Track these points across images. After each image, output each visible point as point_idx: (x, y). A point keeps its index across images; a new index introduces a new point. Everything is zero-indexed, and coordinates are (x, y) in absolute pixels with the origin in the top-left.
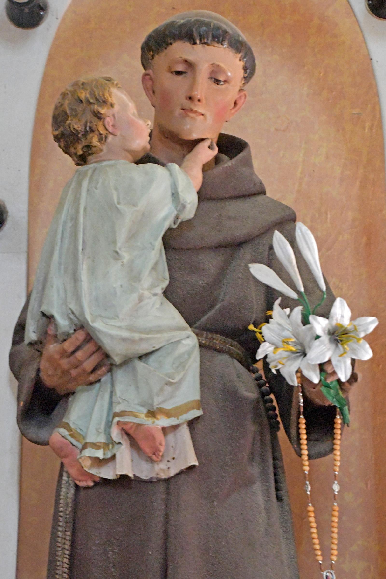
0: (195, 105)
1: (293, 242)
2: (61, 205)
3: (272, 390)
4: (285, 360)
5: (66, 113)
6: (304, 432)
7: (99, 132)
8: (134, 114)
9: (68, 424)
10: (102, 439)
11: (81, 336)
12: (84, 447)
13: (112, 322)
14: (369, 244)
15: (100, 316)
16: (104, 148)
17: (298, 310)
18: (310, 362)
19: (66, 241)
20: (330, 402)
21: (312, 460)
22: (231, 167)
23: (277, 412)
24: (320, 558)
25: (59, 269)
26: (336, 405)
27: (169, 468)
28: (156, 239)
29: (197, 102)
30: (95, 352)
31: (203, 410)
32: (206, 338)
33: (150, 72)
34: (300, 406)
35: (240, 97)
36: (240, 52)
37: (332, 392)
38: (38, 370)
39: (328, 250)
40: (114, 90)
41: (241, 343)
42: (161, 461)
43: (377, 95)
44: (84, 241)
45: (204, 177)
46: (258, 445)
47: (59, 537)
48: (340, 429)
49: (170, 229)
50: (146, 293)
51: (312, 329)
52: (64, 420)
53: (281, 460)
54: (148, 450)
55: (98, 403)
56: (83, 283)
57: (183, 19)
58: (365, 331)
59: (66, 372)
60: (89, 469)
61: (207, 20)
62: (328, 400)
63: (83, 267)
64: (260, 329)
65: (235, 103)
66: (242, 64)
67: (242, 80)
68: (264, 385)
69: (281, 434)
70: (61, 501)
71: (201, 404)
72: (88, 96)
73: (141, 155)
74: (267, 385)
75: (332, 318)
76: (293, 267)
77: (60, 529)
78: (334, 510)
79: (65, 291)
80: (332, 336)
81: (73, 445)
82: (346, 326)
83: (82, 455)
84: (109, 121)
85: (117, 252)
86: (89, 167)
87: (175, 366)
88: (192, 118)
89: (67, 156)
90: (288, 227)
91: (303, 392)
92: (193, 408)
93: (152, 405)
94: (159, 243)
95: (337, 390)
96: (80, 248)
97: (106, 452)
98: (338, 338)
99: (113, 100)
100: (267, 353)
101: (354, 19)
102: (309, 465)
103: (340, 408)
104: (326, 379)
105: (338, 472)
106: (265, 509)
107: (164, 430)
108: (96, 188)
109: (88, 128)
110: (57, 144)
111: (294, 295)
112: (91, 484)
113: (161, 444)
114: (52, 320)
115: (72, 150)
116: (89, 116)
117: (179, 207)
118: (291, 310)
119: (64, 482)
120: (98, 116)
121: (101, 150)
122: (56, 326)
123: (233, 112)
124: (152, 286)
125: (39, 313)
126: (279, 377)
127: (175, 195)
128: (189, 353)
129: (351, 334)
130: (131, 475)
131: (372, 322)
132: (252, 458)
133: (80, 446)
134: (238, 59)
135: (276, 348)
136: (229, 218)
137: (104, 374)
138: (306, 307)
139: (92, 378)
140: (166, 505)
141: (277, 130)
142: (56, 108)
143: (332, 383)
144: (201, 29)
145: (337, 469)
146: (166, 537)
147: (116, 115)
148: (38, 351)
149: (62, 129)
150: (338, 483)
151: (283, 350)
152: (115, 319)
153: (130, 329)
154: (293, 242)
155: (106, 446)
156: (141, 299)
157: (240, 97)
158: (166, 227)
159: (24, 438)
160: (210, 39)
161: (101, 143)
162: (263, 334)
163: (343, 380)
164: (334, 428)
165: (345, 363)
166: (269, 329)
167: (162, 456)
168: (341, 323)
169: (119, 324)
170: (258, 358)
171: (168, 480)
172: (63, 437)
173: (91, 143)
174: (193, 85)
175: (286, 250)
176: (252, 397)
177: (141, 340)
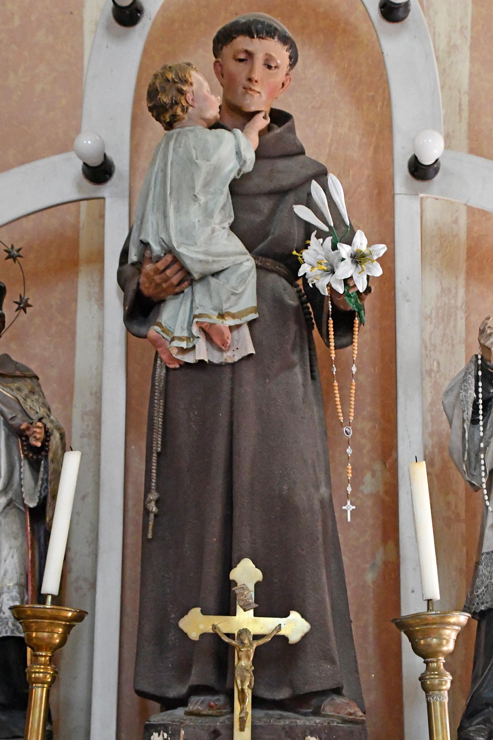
0: (253, 85)
1: (326, 189)
2: (154, 160)
3: (308, 300)
4: (319, 276)
5: (157, 90)
6: (332, 329)
7: (182, 104)
8: (208, 91)
9: (161, 323)
11: (169, 258)
12: (173, 339)
13: (191, 248)
14: (379, 193)
15: (183, 243)
16: (186, 116)
17: (329, 240)
18: (337, 278)
19: (158, 188)
20: (351, 308)
21: (337, 350)
22: (280, 133)
23: (312, 316)
24: (342, 419)
25: (153, 208)
26: (356, 310)
27: (234, 355)
28: (224, 186)
29: (254, 83)
30: (180, 270)
31: (259, 314)
32: (261, 261)
33: (220, 60)
34: (329, 311)
35: (287, 80)
36: (286, 45)
37: (353, 300)
38: (138, 284)
39: (350, 198)
40: (193, 73)
41: (287, 265)
42: (228, 350)
43: (387, 82)
44: (171, 187)
45: (260, 140)
46: (298, 340)
47: (155, 403)
48: (358, 327)
49: (234, 180)
50: (217, 227)
51: (339, 253)
52: (157, 320)
53: (315, 350)
55: (182, 308)
56: (170, 218)
57: (244, 19)
58: (377, 255)
59: (158, 285)
60: (176, 356)
61: (262, 19)
62: (349, 306)
63: (170, 207)
64: (301, 254)
65: (283, 84)
66: (288, 54)
67: (288, 66)
68: (303, 296)
69: (315, 332)
70: (156, 378)
71: (257, 309)
72: (174, 76)
73: (213, 122)
74: (305, 296)
75: (354, 245)
76: (325, 208)
77: (156, 398)
78: (352, 385)
79: (158, 224)
80: (354, 259)
81: (164, 338)
82: (364, 251)
83: (171, 345)
84: (189, 96)
85: (195, 196)
86: (175, 131)
87: (238, 281)
88: (252, 95)
89: (158, 123)
90: (322, 179)
91: (331, 301)
92: (252, 312)
93: (222, 310)
94: (226, 189)
95: (356, 299)
96: (168, 192)
97: (188, 344)
98: (358, 260)
99: (192, 80)
100: (306, 272)
101: (371, 23)
102: (335, 354)
103: (358, 312)
104: (348, 291)
105: (356, 358)
106: (303, 385)
107: (231, 328)
108: (180, 147)
109: (174, 101)
110: (150, 114)
111: (326, 229)
112: (178, 366)
113: (228, 338)
114: (148, 246)
115: (162, 118)
116: (174, 93)
117: (242, 162)
118: (324, 241)
119: (158, 365)
120: (181, 92)
121: (184, 119)
123: (281, 91)
124: (222, 222)
125: (139, 241)
127: (238, 153)
128: (249, 272)
129: (368, 257)
130: (206, 360)
131: (382, 248)
132: (293, 349)
133: (170, 339)
134: (285, 50)
135: (313, 267)
136: (279, 172)
137: (186, 288)
138: (335, 238)
139: (177, 290)
140: (232, 382)
141: (313, 107)
142: (150, 86)
143: (352, 293)
144: (258, 27)
145: (355, 356)
147: (194, 93)
148: (139, 269)
149: (153, 103)
150: (355, 366)
151: (318, 269)
152: (194, 246)
153: (206, 253)
154: (326, 189)
155: (188, 339)
156: (213, 231)
157: (287, 80)
158: (232, 177)
159: (130, 334)
160: (264, 34)
161: (183, 113)
162: (303, 258)
163: (361, 291)
164: (353, 327)
165: (362, 278)
166: (307, 253)
167: (229, 346)
168: (360, 249)
169: (197, 249)
170: (299, 275)
171: (233, 365)
172: (157, 332)
173: (176, 112)
174: (251, 70)
175: (321, 195)
176: (295, 305)
177: (214, 261)
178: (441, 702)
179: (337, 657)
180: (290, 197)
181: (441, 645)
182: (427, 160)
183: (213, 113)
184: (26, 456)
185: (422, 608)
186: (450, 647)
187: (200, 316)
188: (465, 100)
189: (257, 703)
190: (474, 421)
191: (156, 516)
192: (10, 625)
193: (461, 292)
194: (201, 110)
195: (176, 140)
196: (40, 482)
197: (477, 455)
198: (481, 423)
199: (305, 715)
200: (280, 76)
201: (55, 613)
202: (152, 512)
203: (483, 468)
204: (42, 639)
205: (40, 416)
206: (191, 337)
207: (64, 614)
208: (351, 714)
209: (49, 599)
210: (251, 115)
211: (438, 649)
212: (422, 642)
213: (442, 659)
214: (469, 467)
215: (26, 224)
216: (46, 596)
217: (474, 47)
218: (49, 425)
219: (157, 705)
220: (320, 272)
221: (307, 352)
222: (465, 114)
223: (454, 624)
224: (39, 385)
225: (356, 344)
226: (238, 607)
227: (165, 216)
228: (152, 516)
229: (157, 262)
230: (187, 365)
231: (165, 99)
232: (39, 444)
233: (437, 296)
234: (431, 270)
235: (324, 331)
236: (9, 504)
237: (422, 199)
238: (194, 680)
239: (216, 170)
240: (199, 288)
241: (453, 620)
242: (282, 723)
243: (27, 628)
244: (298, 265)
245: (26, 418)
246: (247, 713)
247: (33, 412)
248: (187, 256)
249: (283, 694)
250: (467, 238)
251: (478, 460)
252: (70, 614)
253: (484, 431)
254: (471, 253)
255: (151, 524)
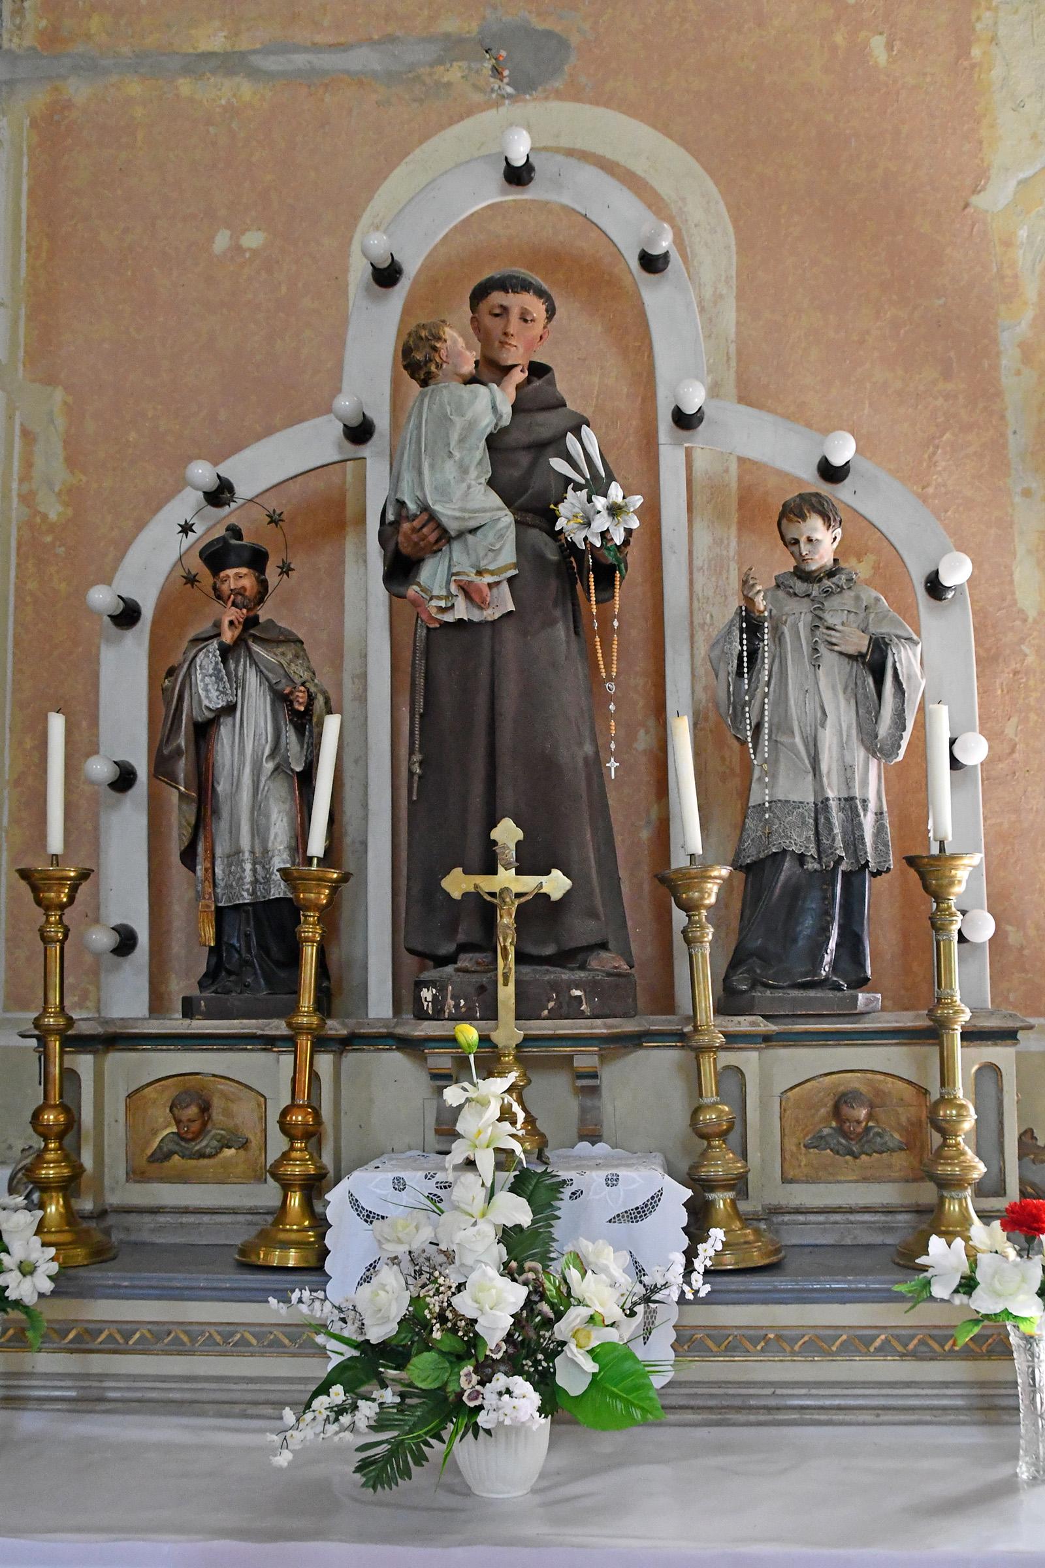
10: (444, 593)
11: (425, 517)
12: (431, 599)
13: (447, 505)
16: (440, 373)
24: (604, 675)
38: (397, 543)
40: (447, 329)
49: (491, 434)
51: (594, 506)
54: (477, 600)
59: (416, 544)
65: (541, 337)
69: (579, 586)
71: (516, 566)
73: (469, 377)
84: (443, 353)
99: (447, 337)
107: (490, 585)
111: (583, 481)
116: (428, 350)
120: (435, 349)
122: (408, 509)
124: (478, 477)
126: (572, 544)
127: (494, 408)
128: (507, 527)
132: (555, 605)
137: (443, 546)
146: (493, 663)
153: (463, 510)
155: (446, 598)
156: (469, 487)
158: (488, 431)
163: (618, 544)
166: (564, 507)
171: (493, 622)
177: (470, 518)
178: (702, 954)
179: (601, 909)
180: (550, 450)
181: (702, 898)
182: (690, 409)
183: (468, 368)
184: (291, 721)
185: (684, 862)
186: (712, 900)
187: (457, 574)
188: (733, 348)
189: (521, 958)
190: (740, 674)
191: (420, 777)
192: (282, 886)
193: (734, 543)
194: (456, 366)
195: (430, 397)
196: (305, 746)
197: (743, 708)
198: (746, 675)
199: (572, 969)
200: (538, 328)
201: (321, 874)
202: (415, 773)
203: (748, 721)
204: (310, 900)
205: (303, 680)
206: (450, 596)
207: (330, 875)
208: (616, 968)
209: (315, 860)
210: (509, 369)
211: (699, 903)
212: (684, 896)
213: (704, 912)
214: (734, 720)
215: (294, 487)
216: (311, 858)
217: (740, 297)
218: (313, 689)
219: (431, 963)
220: (577, 525)
221: (570, 606)
222: (733, 363)
223: (715, 878)
224: (304, 650)
225: (617, 599)
226: (499, 866)
227: (420, 473)
228: (416, 778)
229: (414, 520)
230: (445, 625)
231: (419, 356)
232: (302, 709)
233: (709, 547)
234: (357, 561)
235: (586, 585)
236: (276, 769)
237: (686, 448)
238: (461, 937)
239: (470, 426)
240: (456, 546)
241: (715, 873)
242: (547, 978)
243: (294, 889)
244: (555, 518)
245: (290, 683)
246: (510, 969)
247: (296, 677)
248: (443, 514)
249: (549, 950)
250: (738, 489)
251: (744, 713)
252: (335, 876)
253: (749, 684)
254: (742, 502)
255: (415, 785)
